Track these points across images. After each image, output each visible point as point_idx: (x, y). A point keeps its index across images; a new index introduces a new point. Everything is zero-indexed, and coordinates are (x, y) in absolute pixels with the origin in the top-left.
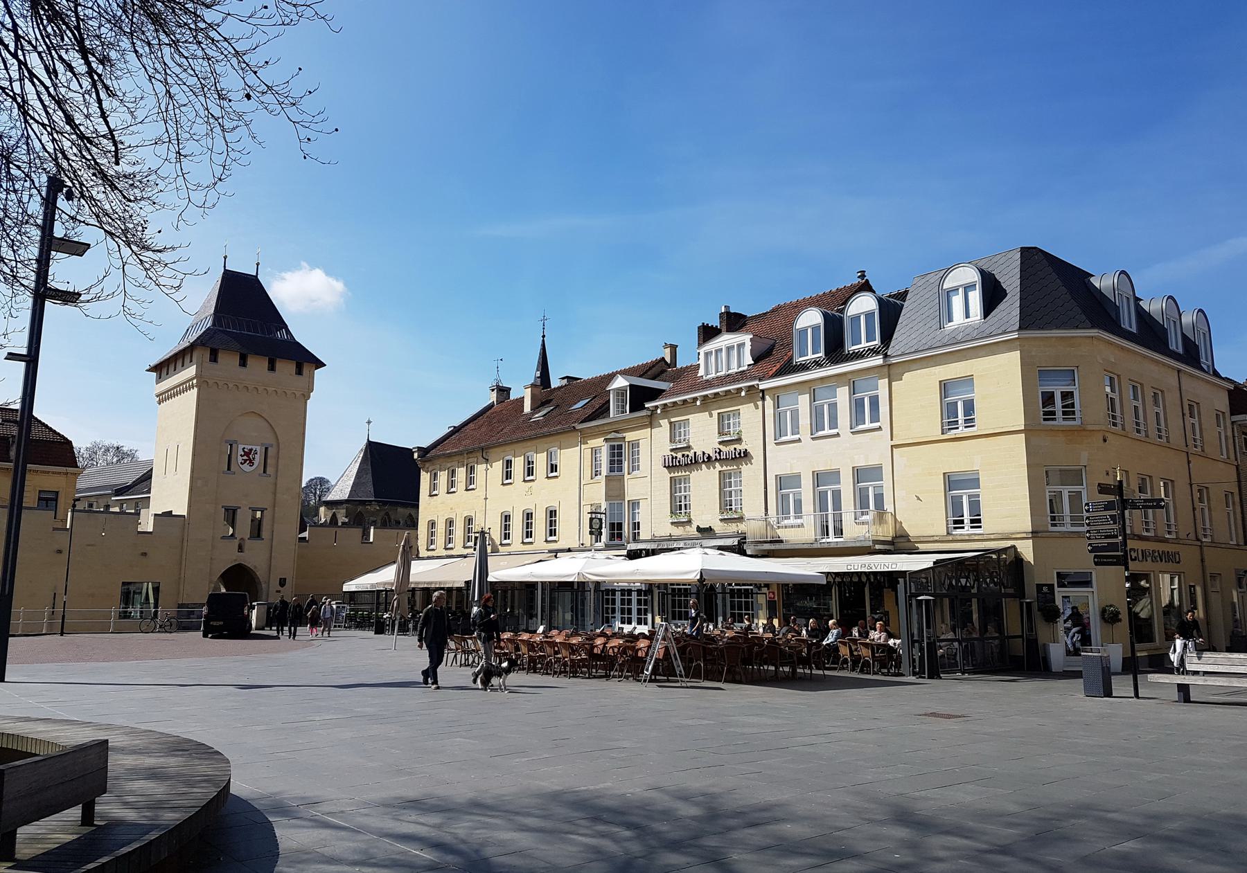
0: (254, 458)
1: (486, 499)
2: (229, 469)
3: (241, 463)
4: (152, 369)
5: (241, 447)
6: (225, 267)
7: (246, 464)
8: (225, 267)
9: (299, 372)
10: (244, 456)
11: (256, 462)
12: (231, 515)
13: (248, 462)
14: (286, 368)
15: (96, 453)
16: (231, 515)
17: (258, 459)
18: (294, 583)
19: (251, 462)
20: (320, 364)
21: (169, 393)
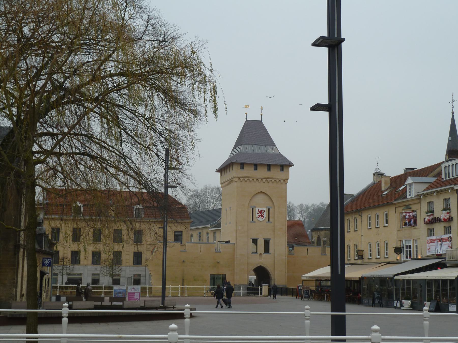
0: (263, 214)
1: (362, 236)
2: (252, 220)
3: (258, 217)
4: (217, 171)
5: (257, 209)
6: (246, 118)
7: (260, 217)
8: (246, 118)
9: (282, 170)
10: (259, 213)
11: (265, 216)
12: (255, 241)
13: (261, 216)
14: (275, 173)
15: (207, 192)
16: (255, 241)
17: (265, 215)
18: (286, 275)
19: (262, 216)
20: (291, 165)
21: (225, 183)
